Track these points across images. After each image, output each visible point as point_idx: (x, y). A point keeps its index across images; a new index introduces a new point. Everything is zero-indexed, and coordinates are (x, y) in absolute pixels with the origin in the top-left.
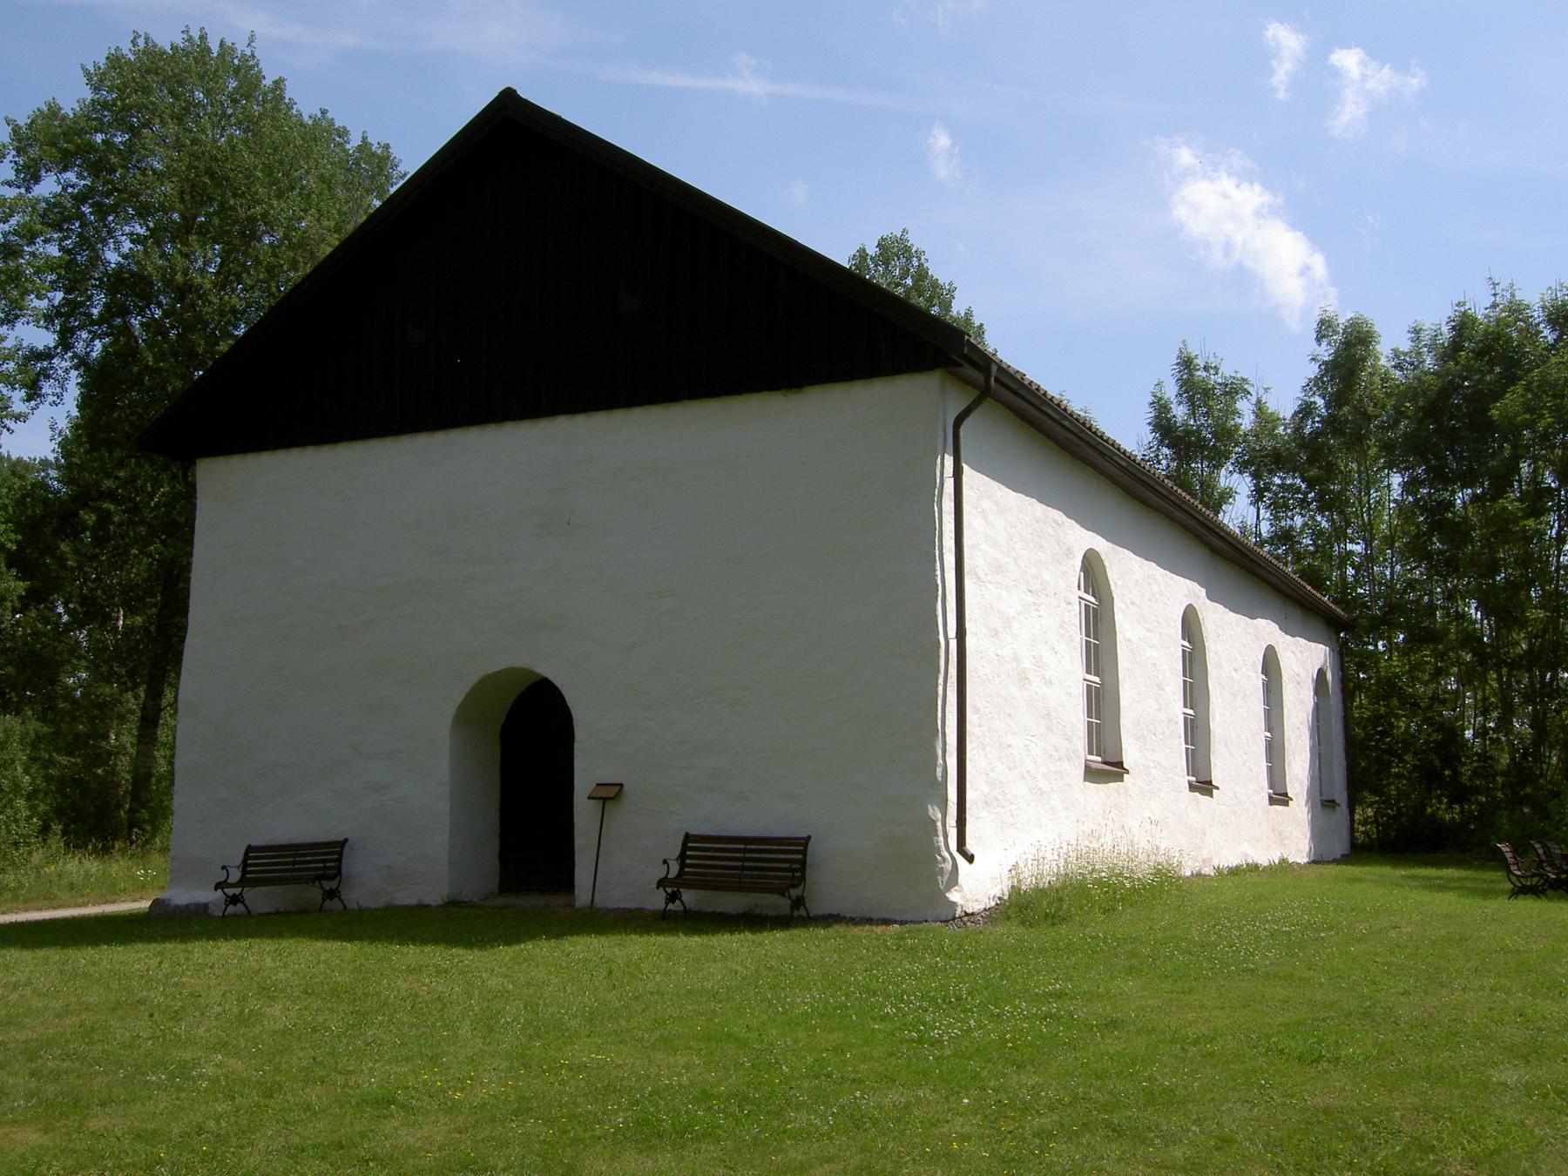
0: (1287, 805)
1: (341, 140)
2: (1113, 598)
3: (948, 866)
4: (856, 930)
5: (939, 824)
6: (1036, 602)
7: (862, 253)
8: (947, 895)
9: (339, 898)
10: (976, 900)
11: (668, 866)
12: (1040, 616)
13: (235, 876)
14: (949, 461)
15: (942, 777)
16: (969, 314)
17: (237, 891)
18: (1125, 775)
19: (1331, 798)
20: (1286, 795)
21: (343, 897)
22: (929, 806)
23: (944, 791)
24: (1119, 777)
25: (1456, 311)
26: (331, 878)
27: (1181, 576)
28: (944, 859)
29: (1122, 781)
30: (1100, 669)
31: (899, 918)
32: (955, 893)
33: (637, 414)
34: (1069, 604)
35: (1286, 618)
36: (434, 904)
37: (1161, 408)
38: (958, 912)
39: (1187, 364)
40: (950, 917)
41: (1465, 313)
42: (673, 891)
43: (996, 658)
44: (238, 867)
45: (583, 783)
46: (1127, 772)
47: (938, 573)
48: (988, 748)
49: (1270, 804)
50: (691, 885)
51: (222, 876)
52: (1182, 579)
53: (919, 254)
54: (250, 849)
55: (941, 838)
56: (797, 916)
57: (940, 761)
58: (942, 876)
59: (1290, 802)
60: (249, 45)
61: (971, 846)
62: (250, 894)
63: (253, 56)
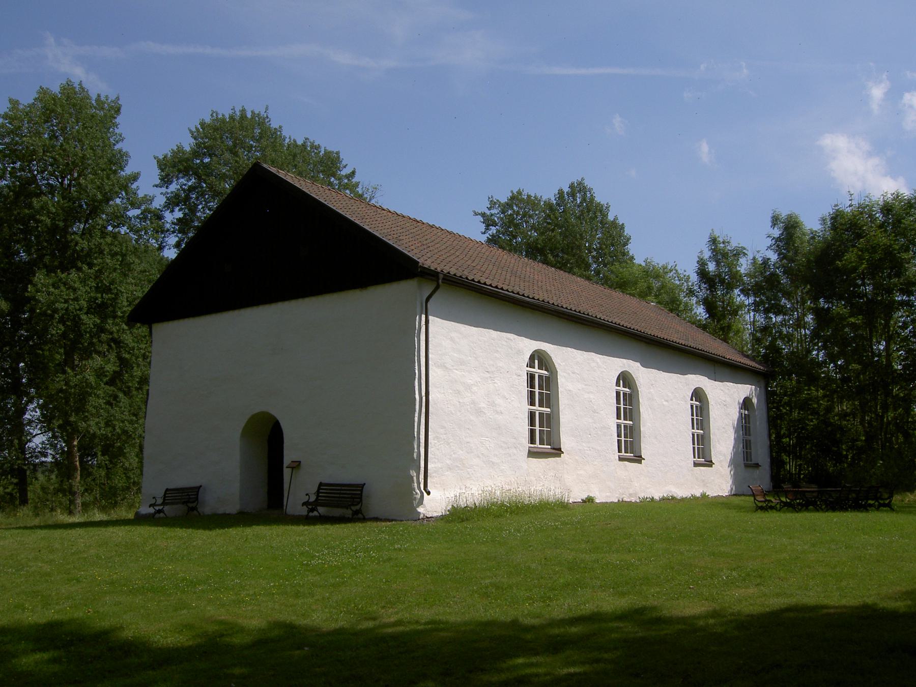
0: (712, 467)
1: (317, 151)
2: (557, 371)
3: (418, 496)
4: (375, 524)
5: (415, 478)
6: (492, 376)
7: (561, 193)
8: (417, 509)
9: (197, 510)
10: (435, 511)
11: (309, 496)
12: (494, 383)
13: (160, 501)
14: (423, 316)
15: (417, 457)
16: (616, 218)
17: (161, 507)
18: (562, 454)
19: (756, 462)
20: (711, 461)
21: (198, 510)
22: (411, 471)
23: (418, 464)
24: (559, 455)
25: (833, 209)
26: (193, 502)
27: (617, 357)
28: (417, 493)
29: (560, 457)
30: (551, 405)
31: (399, 519)
32: (421, 508)
33: (300, 301)
34: (519, 376)
35: (715, 373)
36: (234, 513)
37: (702, 264)
38: (421, 516)
39: (714, 241)
40: (416, 518)
41: (837, 210)
42: (312, 508)
43: (458, 403)
44: (161, 498)
45: (287, 461)
46: (563, 453)
47: (417, 367)
48: (451, 444)
49: (694, 466)
50: (323, 505)
51: (153, 501)
52: (618, 359)
53: (590, 190)
54: (321, 484)
55: (416, 484)
56: (358, 517)
57: (416, 450)
58: (415, 501)
59: (713, 465)
60: (265, 112)
61: (429, 489)
62: (166, 508)
63: (267, 117)
